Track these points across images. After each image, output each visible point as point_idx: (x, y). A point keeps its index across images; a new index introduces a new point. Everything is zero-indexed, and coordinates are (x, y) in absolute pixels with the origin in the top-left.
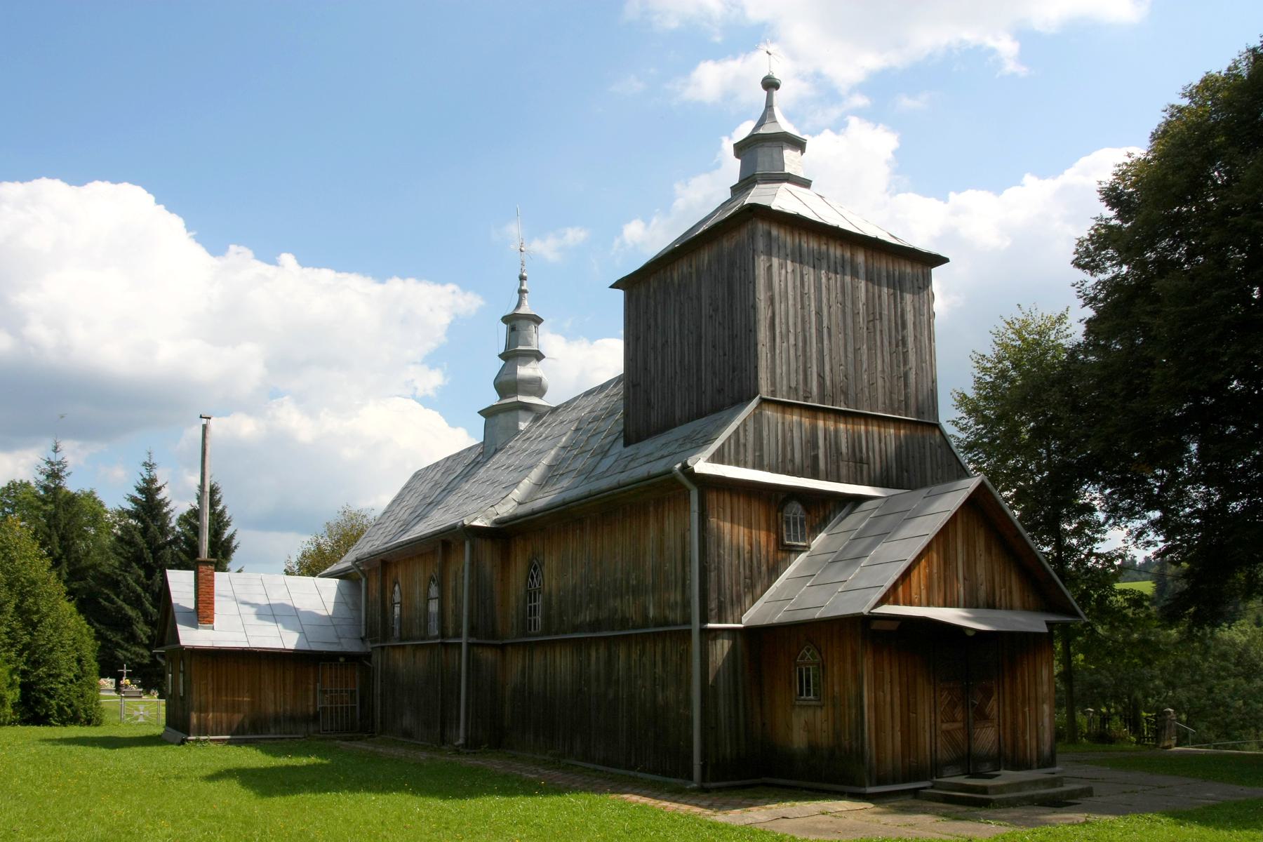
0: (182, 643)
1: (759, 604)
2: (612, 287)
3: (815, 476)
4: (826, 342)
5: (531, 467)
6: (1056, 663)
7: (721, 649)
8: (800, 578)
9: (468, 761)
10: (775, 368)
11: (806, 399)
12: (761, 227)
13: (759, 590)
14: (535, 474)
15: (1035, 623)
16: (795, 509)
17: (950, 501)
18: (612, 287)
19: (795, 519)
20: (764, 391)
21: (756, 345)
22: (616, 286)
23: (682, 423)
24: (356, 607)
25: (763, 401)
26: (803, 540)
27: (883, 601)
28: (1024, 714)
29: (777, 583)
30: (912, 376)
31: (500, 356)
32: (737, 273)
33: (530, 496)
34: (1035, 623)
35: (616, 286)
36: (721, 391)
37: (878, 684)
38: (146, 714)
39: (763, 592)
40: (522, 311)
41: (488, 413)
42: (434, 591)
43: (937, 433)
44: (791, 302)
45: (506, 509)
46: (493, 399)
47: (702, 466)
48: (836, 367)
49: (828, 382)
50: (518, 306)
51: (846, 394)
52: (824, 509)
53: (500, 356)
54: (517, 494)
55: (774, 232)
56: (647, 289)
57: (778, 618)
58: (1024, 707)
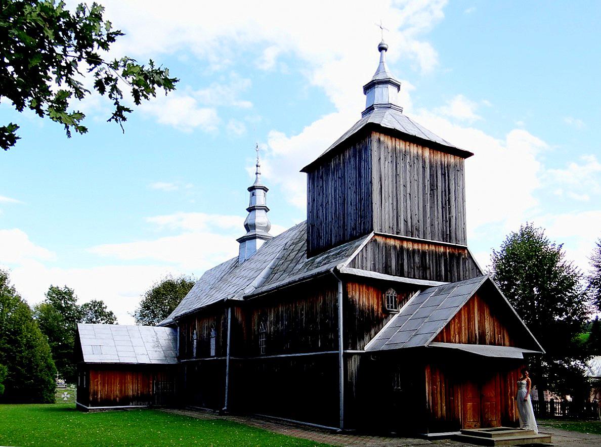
0: (85, 361)
1: (373, 341)
2: (300, 171)
3: (402, 275)
4: (408, 202)
5: (262, 269)
6: (88, 408)
7: (354, 365)
8: (395, 327)
9: (231, 419)
10: (382, 216)
11: (398, 233)
12: (375, 136)
13: (373, 332)
14: (264, 273)
15: (517, 353)
16: (392, 293)
17: (468, 289)
18: (300, 171)
19: (391, 297)
20: (376, 230)
21: (372, 203)
22: (303, 171)
23: (335, 245)
24: (175, 340)
25: (376, 234)
26: (396, 308)
27: (436, 340)
28: (512, 399)
29: (383, 330)
30: (453, 220)
31: (247, 209)
32: (363, 163)
33: (262, 284)
34: (517, 353)
35: (303, 171)
36: (354, 229)
37: (433, 382)
38: (69, 396)
39: (376, 334)
40: (258, 185)
41: (242, 240)
42: (213, 333)
43: (466, 251)
44: (390, 180)
45: (249, 291)
46: (244, 233)
47: (344, 267)
48: (414, 217)
49: (409, 224)
50: (256, 182)
51: (418, 230)
52: (405, 291)
53: (247, 209)
54: (256, 283)
55: (382, 139)
56: (316, 171)
57: (384, 348)
58: (511, 396)
